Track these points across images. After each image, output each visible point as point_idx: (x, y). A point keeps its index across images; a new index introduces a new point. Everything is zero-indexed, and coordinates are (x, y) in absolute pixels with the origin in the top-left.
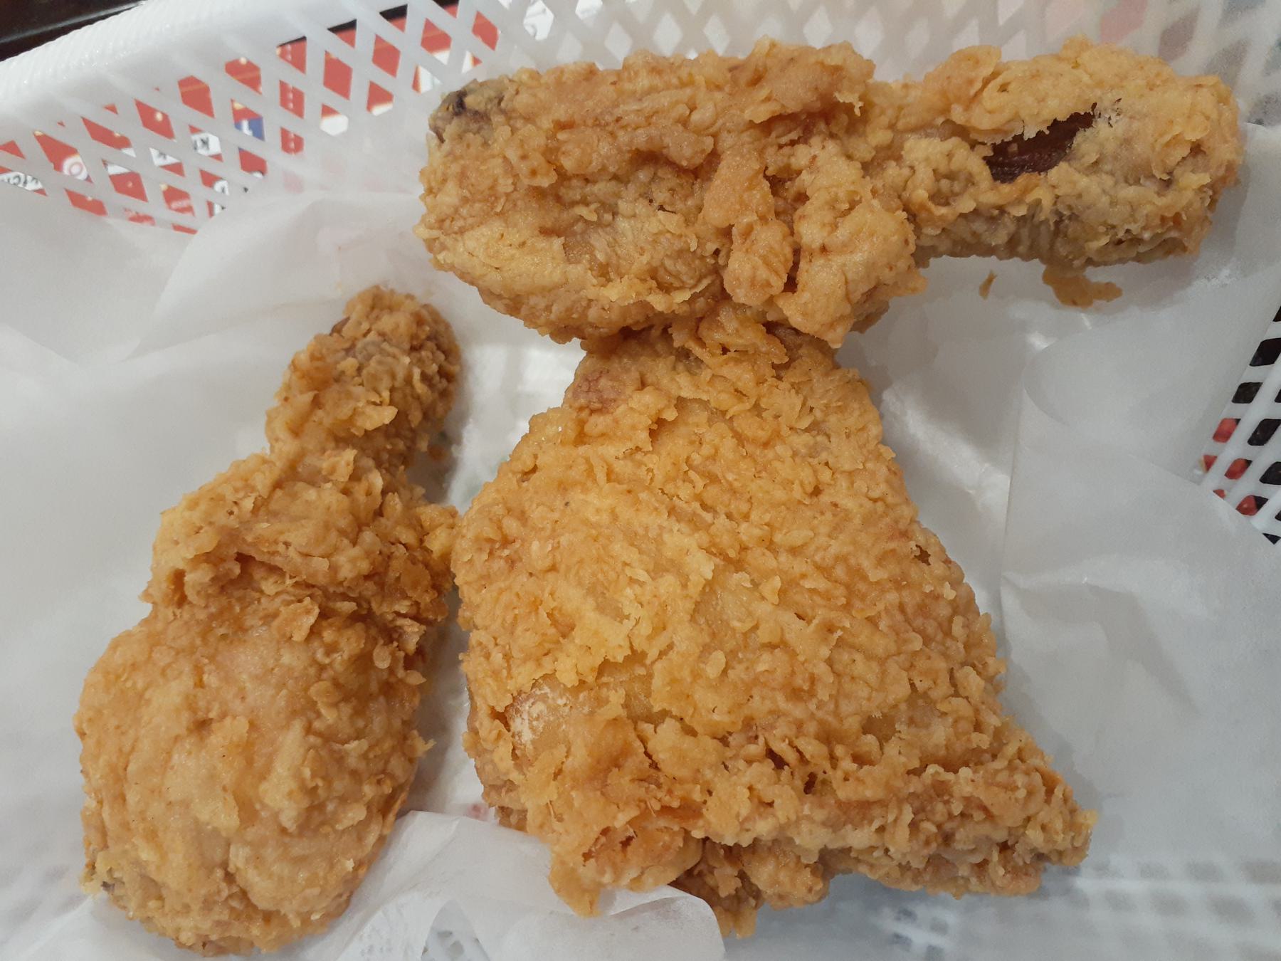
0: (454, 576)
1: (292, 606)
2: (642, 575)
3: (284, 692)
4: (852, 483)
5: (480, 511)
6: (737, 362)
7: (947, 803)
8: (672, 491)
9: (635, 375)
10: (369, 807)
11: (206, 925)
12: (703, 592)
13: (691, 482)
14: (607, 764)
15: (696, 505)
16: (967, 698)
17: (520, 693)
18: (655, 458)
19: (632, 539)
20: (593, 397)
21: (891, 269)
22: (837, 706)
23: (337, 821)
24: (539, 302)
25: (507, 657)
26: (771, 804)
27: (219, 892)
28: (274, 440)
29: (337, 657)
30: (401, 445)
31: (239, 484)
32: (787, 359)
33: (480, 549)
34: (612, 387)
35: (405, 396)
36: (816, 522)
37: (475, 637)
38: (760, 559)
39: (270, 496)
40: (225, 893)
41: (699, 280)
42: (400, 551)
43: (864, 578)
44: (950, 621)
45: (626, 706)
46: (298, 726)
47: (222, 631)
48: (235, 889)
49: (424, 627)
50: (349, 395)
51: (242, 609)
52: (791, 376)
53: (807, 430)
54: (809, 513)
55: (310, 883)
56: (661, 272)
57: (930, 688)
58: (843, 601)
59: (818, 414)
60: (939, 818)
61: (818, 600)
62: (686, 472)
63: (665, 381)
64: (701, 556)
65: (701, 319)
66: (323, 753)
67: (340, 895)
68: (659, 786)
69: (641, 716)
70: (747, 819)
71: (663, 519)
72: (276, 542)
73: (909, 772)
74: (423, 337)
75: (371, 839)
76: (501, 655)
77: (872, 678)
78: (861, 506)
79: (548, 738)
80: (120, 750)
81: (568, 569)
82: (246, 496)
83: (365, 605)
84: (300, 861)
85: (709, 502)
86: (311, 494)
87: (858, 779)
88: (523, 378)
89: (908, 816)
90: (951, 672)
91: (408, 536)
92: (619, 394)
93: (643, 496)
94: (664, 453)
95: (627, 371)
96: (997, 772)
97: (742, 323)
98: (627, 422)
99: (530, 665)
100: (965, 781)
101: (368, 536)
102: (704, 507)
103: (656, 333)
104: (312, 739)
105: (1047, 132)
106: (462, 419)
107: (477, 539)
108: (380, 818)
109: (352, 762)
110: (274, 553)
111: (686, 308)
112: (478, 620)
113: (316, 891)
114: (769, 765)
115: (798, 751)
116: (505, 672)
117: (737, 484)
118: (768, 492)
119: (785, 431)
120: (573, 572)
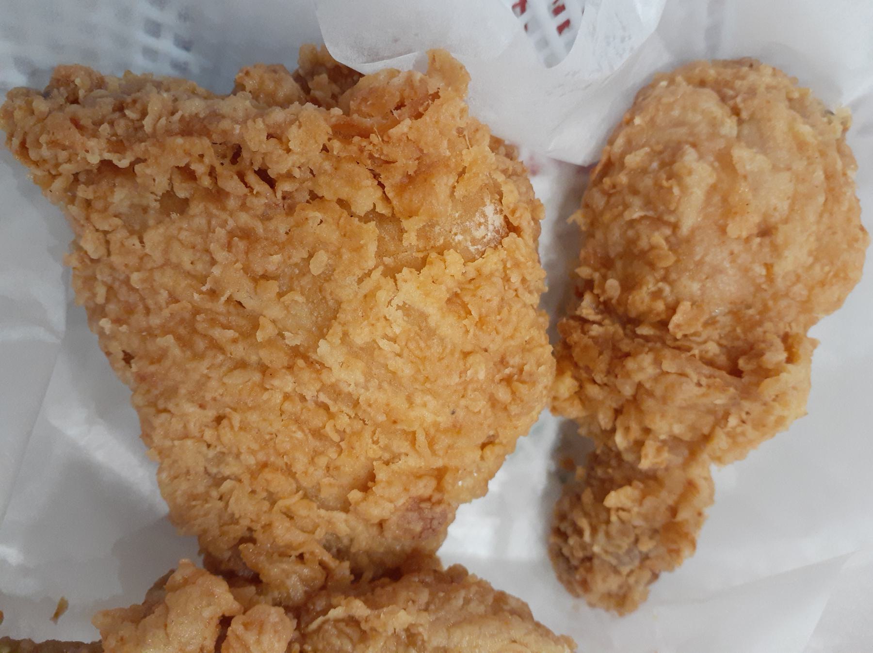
0: (553, 353)
1: (692, 331)
2: (384, 344)
3: (697, 258)
4: (185, 427)
5: (532, 409)
6: (289, 546)
7: (115, 135)
8: (355, 422)
9: (388, 534)
10: (622, 166)
11: (752, 77)
12: (329, 327)
13: (337, 431)
14: (419, 176)
15: (333, 409)
16: (97, 230)
17: (496, 247)
18: (371, 454)
19: (394, 377)
20: (427, 513)
21: (122, 639)
22: (209, 223)
23: (648, 154)
24: (477, 608)
25: (507, 279)
26: (270, 136)
27: (744, 100)
28: (708, 479)
29: (652, 287)
30: (600, 472)
31: (741, 439)
32: (241, 547)
33: (531, 375)
34: (409, 523)
35: (597, 516)
36: (221, 391)
37: (535, 299)
38: (276, 358)
39: (713, 428)
40: (739, 100)
41: (320, 628)
42: (599, 378)
43: (179, 338)
44: (108, 300)
45: (402, 231)
46: (685, 230)
47: (751, 312)
48: (731, 103)
49: (578, 313)
50: (645, 518)
51: (735, 330)
52: (238, 531)
53: (224, 479)
54: (227, 399)
55: (670, 107)
56: (356, 636)
57: (127, 238)
58: (198, 318)
59: (215, 494)
60: (122, 122)
61: (222, 319)
62: (342, 440)
63: (360, 528)
64: (330, 361)
65: (324, 587)
66: (662, 208)
67: (644, 99)
68: (371, 157)
69: (389, 220)
70: (292, 122)
71: (364, 396)
72: (709, 386)
73: (145, 161)
74: (581, 570)
75: (620, 141)
76: (513, 280)
77: (176, 246)
78: (177, 405)
79: (471, 206)
80: (831, 214)
81: (452, 353)
82: (734, 428)
83: (628, 331)
84: (679, 123)
85: (322, 411)
86: (678, 429)
87: (190, 155)
88: (493, 532)
89: (148, 123)
90: (109, 254)
91: (593, 391)
92: (403, 516)
93: (381, 418)
94: (363, 459)
95: (395, 538)
96: (69, 161)
97: (283, 583)
98: (396, 490)
99: (486, 270)
100: (95, 152)
101: (628, 390)
102: (326, 408)
103: (368, 575)
104: (672, 219)
106: (547, 495)
107: (534, 383)
108: (613, 158)
109: (636, 202)
110: (710, 377)
111: (334, 601)
112: (532, 313)
113: (665, 100)
114: (272, 173)
115: (246, 184)
116: (509, 265)
117: (294, 428)
118: (264, 420)
119: (246, 478)
120: (448, 351)
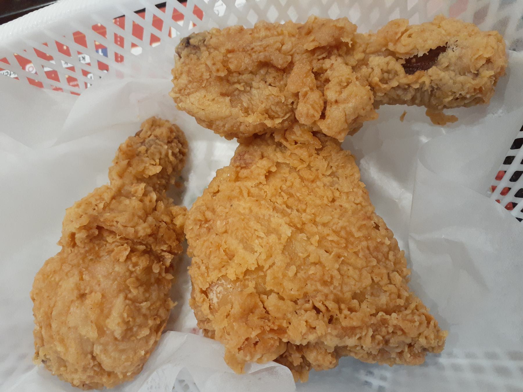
0: (185, 235)
1: (119, 247)
2: (262, 235)
3: (116, 282)
4: (348, 197)
5: (196, 209)
6: (301, 147)
7: (387, 327)
8: (275, 200)
9: (259, 153)
10: (151, 329)
11: (84, 377)
12: (287, 242)
13: (282, 196)
14: (248, 312)
15: (284, 206)
16: (395, 285)
17: (212, 283)
18: (267, 187)
19: (258, 220)
20: (242, 162)
21: (364, 110)
22: (342, 288)
23: (138, 335)
24: (220, 123)
25: (207, 268)
26: (315, 328)
27: (89, 364)
28: (112, 179)
29: (138, 268)
30: (164, 182)
31: (98, 197)
32: (321, 147)
33: (196, 224)
34: (250, 158)
35: (165, 162)
36: (333, 213)
37: (194, 260)
38: (310, 228)
39: (110, 203)
40: (92, 364)
41: (286, 114)
42: (163, 225)
43: (353, 236)
44: (388, 253)
45: (256, 288)
46: (121, 296)
47: (91, 257)
48: (96, 363)
49: (173, 256)
50: (143, 161)
51: (99, 249)
52: (323, 154)
53: (329, 175)
54: (330, 209)
55: (127, 360)
56: (270, 111)
57: (380, 281)
58: (344, 245)
59: (334, 169)
60: (383, 334)
61: (334, 245)
62: (280, 193)
63: (271, 156)
64: (286, 227)
65: (286, 130)
66: (132, 307)
67: (139, 365)
68: (269, 321)
69: (262, 292)
70: (305, 334)
71: (271, 212)
72: (113, 221)
73: (371, 315)
74: (173, 137)
75: (152, 342)
76: (204, 267)
77: (356, 277)
78: (352, 206)
79: (224, 301)
80: (49, 306)
81: (232, 232)
82: (101, 202)
83: (149, 247)
84: (123, 351)
85: (290, 205)
86: (127, 202)
87: (350, 318)
88: (213, 154)
89: (371, 333)
90: (388, 274)
91: (166, 219)
92: (253, 161)
93: (263, 202)
94: (271, 185)
95: (256, 151)
96: (407, 315)
97: (303, 132)
98: (256, 172)
99: (216, 271)
100: (394, 319)
101: (150, 219)
102: (288, 207)
103: (268, 136)
104: (127, 301)
105: (428, 54)
106: (189, 171)
107: (195, 220)
108: (155, 334)
109: (144, 311)
110: (112, 226)
111: (280, 126)
112: (195, 253)
113: (129, 363)
114: (314, 312)
115: (326, 306)
116: (206, 274)
117: (301, 198)
118: (313, 201)
119: (320, 176)
120: (234, 233)
